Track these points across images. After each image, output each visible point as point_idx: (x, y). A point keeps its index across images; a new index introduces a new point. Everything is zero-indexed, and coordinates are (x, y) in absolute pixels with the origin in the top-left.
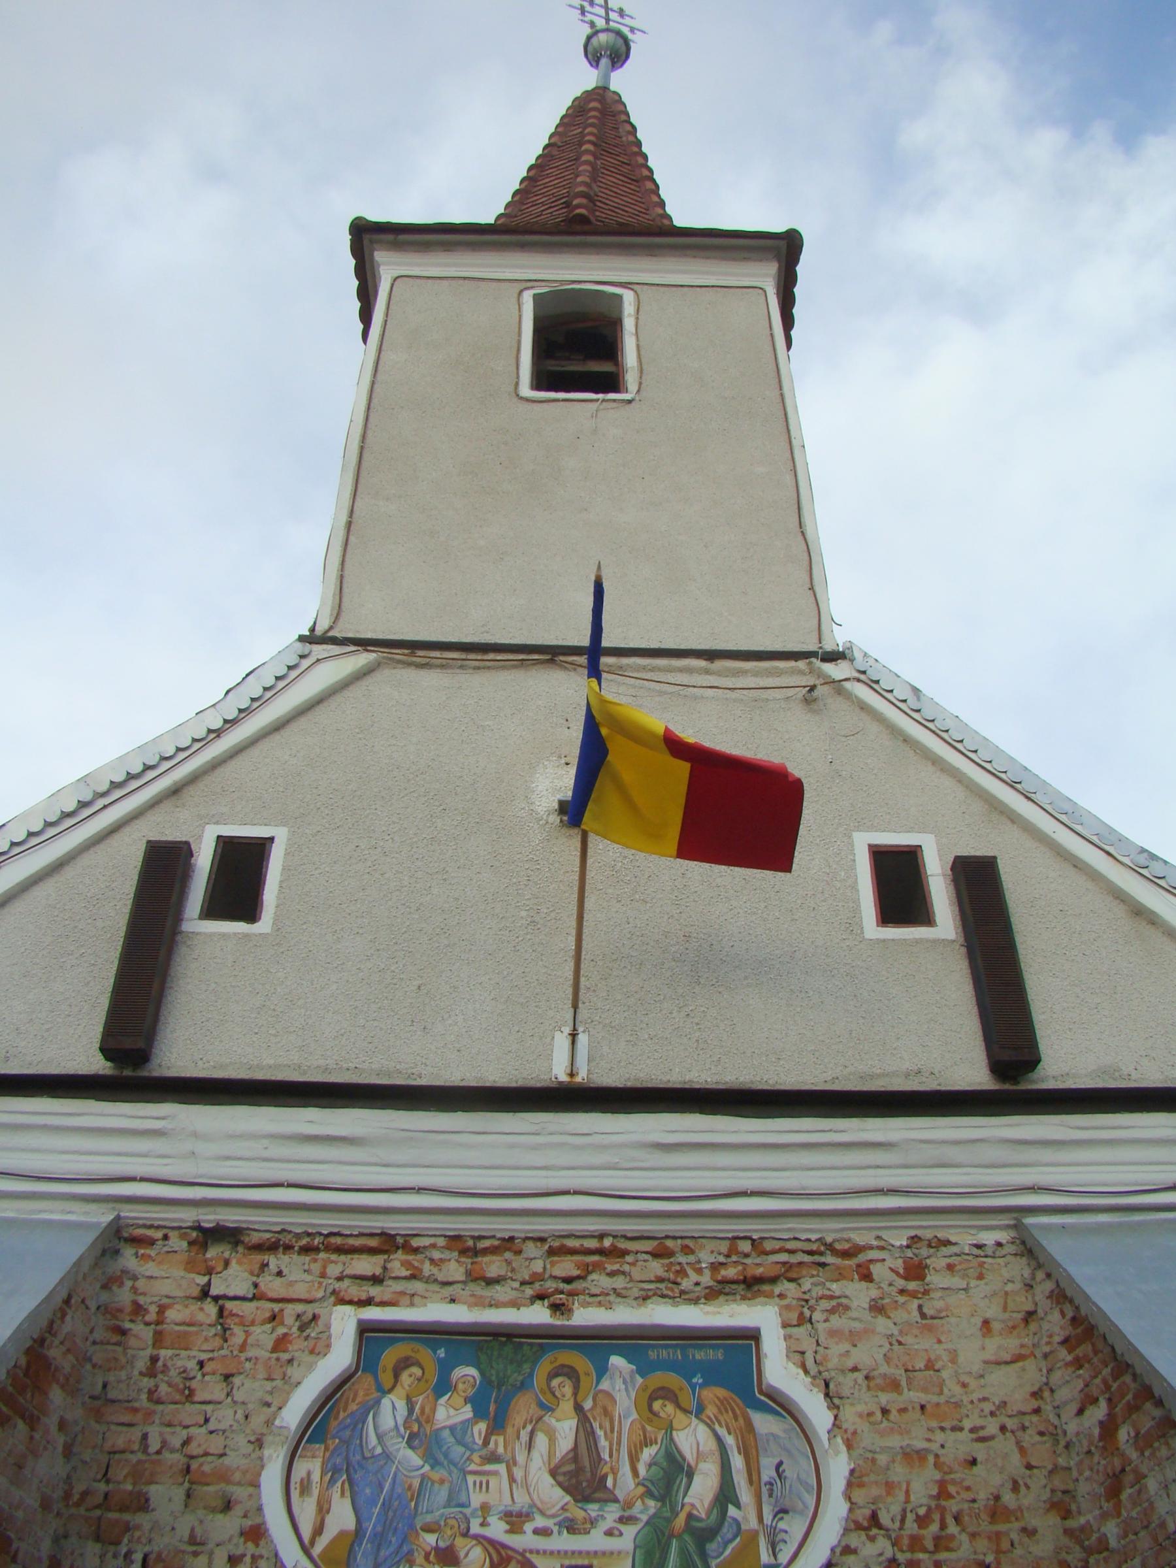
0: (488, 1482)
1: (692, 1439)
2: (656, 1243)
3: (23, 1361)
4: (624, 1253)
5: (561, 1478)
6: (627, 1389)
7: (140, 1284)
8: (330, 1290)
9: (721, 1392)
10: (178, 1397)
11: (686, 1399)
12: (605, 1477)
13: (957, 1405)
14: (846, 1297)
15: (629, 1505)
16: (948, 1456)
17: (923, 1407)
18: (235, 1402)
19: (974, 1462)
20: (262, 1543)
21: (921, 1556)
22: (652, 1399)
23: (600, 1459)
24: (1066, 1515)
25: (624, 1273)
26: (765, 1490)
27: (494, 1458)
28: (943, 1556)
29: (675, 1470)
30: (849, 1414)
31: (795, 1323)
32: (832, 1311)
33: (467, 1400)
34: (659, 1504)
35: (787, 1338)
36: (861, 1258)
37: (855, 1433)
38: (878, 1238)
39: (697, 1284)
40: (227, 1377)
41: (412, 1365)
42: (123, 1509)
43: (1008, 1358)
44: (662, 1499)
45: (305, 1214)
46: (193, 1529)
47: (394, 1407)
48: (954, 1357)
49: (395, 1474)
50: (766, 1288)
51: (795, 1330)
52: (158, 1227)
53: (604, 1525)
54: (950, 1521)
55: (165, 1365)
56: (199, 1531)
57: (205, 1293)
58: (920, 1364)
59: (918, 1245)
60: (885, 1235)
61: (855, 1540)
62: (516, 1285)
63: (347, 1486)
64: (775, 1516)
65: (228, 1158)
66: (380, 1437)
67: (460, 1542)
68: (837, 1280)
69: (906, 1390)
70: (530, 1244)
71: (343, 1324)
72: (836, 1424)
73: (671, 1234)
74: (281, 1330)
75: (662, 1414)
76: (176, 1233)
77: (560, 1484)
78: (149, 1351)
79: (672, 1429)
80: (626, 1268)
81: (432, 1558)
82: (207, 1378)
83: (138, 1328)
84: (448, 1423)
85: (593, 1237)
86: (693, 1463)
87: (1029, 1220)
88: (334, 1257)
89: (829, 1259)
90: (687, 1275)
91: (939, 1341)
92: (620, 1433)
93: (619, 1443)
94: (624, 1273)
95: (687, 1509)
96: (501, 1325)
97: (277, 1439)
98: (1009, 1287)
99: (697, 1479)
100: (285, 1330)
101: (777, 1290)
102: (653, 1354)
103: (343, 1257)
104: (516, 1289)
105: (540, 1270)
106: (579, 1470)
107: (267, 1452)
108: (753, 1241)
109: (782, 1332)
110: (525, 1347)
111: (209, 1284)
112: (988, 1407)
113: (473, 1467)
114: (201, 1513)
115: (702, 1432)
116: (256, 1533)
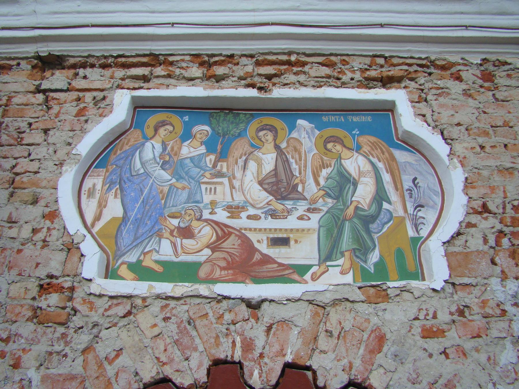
0: (215, 188)
1: (355, 164)
2: (324, 58)
5: (266, 186)
6: (309, 137)
8: (115, 85)
9: (372, 139)
10: (12, 142)
11: (348, 141)
12: (297, 185)
14: (447, 88)
17: (505, 146)
18: (48, 144)
20: (56, 221)
22: (326, 142)
23: (293, 175)
25: (304, 73)
26: (406, 194)
29: (344, 182)
31: (417, 100)
34: (335, 201)
36: (454, 70)
37: (465, 157)
38: (462, 59)
39: (352, 79)
40: (46, 131)
41: (167, 124)
44: (337, 198)
46: (11, 214)
47: (153, 147)
49: (152, 184)
51: (417, 105)
55: (7, 126)
59: (487, 64)
60: (466, 57)
61: (474, 219)
62: (235, 79)
63: (119, 191)
64: (415, 209)
66: (143, 164)
67: (195, 224)
68: (441, 79)
69: (493, 137)
71: (122, 102)
72: (451, 154)
73: (334, 52)
74: (82, 106)
75: (334, 150)
76: (25, 61)
77: (265, 190)
79: (341, 159)
81: (175, 233)
82: (32, 131)
84: (189, 156)
85: (284, 54)
86: (357, 178)
90: (345, 74)
91: (509, 112)
92: (306, 161)
93: (305, 166)
94: (304, 73)
95: (354, 204)
97: (73, 161)
99: (360, 187)
100: (85, 105)
101: (403, 85)
102: (325, 119)
104: (235, 81)
108: (386, 58)
110: (241, 115)
111: (41, 84)
113: (205, 180)
114: (17, 204)
115: (361, 160)
116: (53, 215)
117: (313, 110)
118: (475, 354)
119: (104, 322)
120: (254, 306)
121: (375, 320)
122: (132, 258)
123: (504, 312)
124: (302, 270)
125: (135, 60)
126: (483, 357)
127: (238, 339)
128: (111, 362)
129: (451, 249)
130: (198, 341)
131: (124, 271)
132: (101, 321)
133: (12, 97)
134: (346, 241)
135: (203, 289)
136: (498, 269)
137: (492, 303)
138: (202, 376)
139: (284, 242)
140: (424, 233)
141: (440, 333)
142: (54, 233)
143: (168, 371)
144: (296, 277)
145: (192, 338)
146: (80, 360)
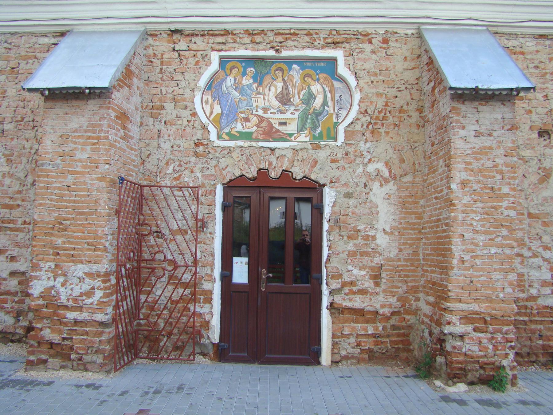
3: (124, 71)
4: (297, 34)
7: (155, 48)
9: (325, 75)
10: (169, 79)
11: (315, 77)
13: (394, 81)
15: (297, 106)
16: (389, 95)
19: (396, 97)
21: (378, 121)
22: (305, 77)
24: (421, 112)
27: (259, 93)
28: (384, 122)
29: (311, 97)
30: (361, 82)
32: (359, 52)
33: (251, 78)
35: (345, 60)
36: (370, 37)
42: (158, 109)
43: (411, 68)
44: (306, 105)
45: (201, 24)
48: (394, 67)
50: (340, 45)
52: (158, 31)
53: (290, 112)
54: (388, 112)
56: (178, 115)
57: (174, 50)
58: (384, 69)
60: (377, 30)
61: (360, 117)
62: (265, 44)
65: (176, 9)
67: (250, 116)
70: (269, 32)
71: (215, 57)
74: (197, 59)
77: (278, 100)
78: (160, 67)
80: (298, 39)
83: (155, 60)
87: (423, 27)
88: (211, 37)
89: (360, 37)
96: (261, 56)
98: (414, 47)
102: (305, 64)
103: (213, 37)
105: (272, 40)
106: (283, 97)
107: (195, 93)
109: (344, 58)
112: (403, 82)
113: (253, 96)
115: (319, 86)
116: (194, 114)
117: (299, 61)
118: (349, 169)
119: (220, 156)
120: (272, 150)
121: (315, 156)
122: (227, 130)
123: (362, 155)
124: (291, 135)
125: (218, 33)
126: (351, 170)
127: (267, 162)
128: (224, 170)
129: (348, 129)
130: (253, 162)
131: (224, 136)
132: (219, 156)
133: (164, 54)
134: (309, 124)
135: (254, 144)
136: (364, 138)
137: (359, 151)
138: (255, 174)
139: (284, 124)
140: (340, 121)
141: (337, 161)
142: (197, 122)
143: (244, 173)
144: (288, 138)
145: (251, 162)
146: (213, 169)
